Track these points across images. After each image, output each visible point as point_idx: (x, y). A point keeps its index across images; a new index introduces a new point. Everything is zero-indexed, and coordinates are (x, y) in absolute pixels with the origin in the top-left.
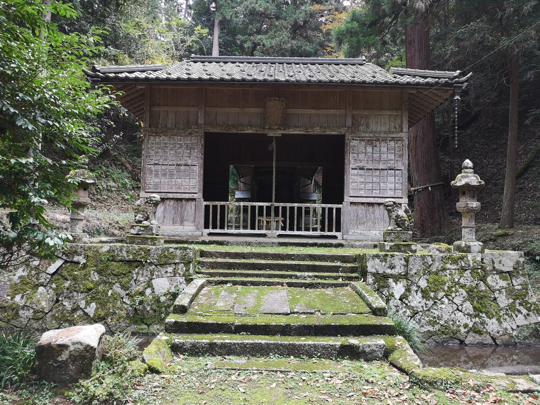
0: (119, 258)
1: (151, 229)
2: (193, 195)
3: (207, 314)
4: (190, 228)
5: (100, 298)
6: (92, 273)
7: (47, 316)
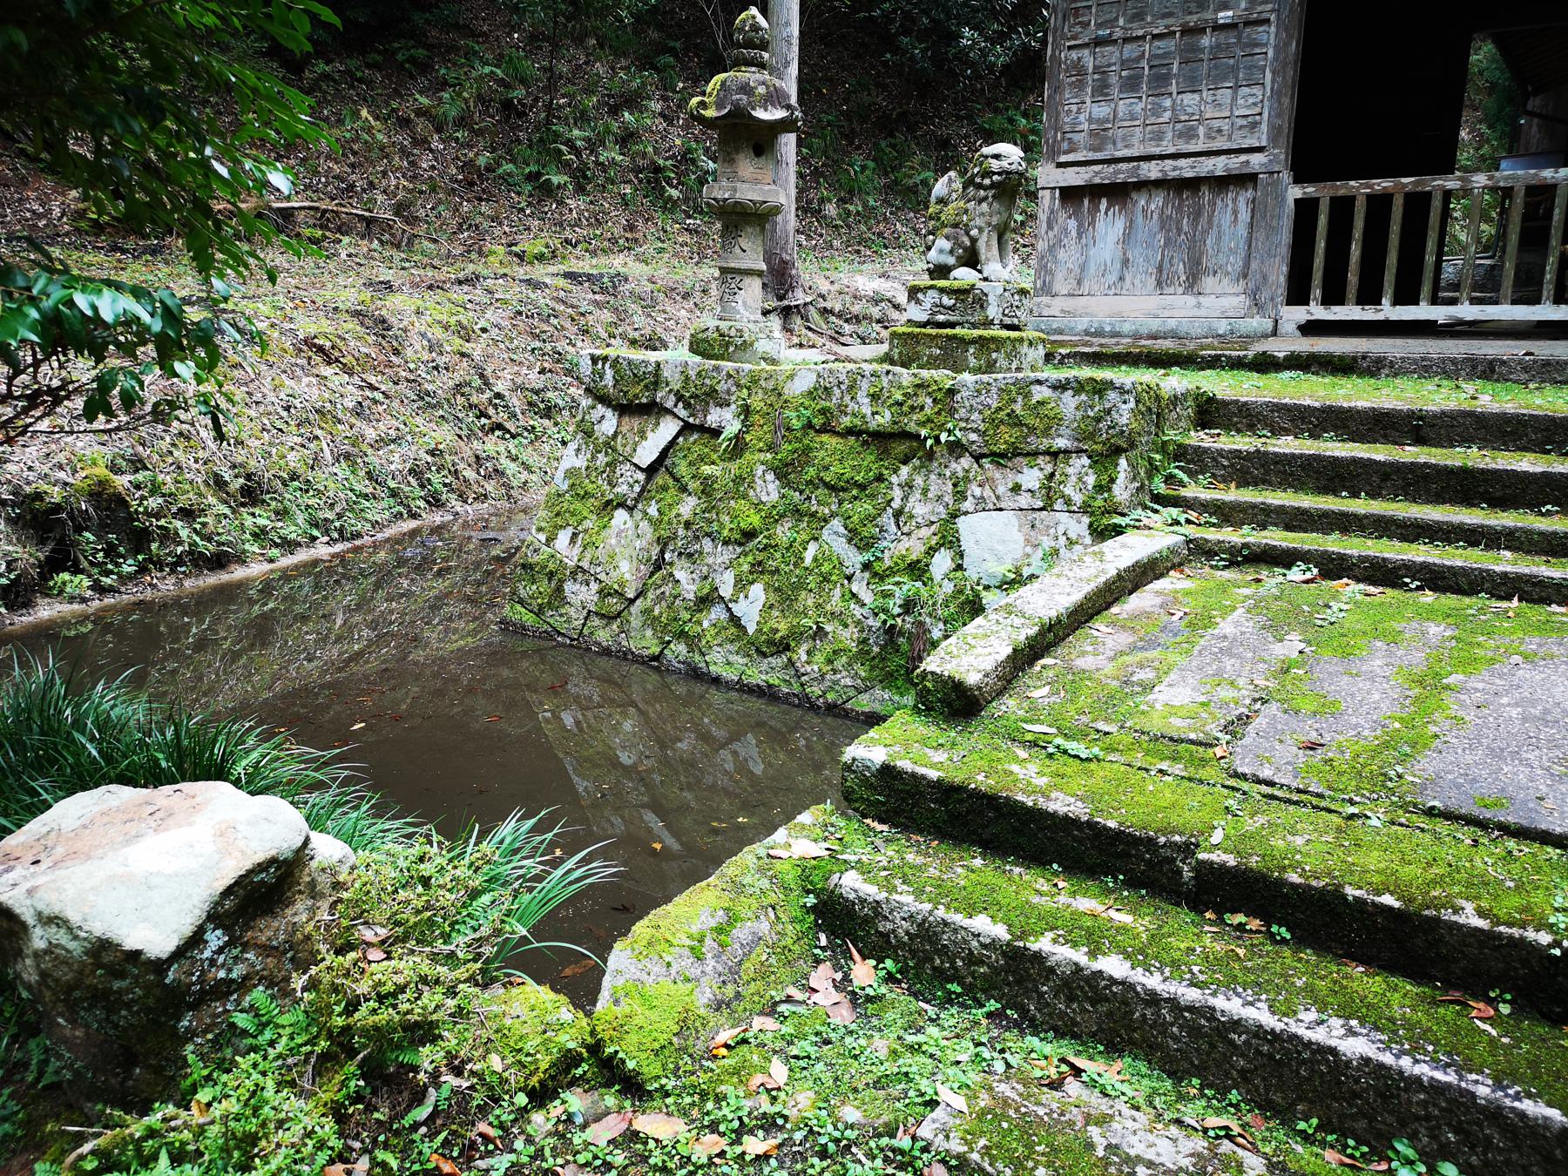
0: (846, 421)
1: (981, 302)
2: (1243, 158)
3: (1073, 746)
4: (1226, 302)
5: (777, 570)
6: (760, 473)
7: (633, 609)
